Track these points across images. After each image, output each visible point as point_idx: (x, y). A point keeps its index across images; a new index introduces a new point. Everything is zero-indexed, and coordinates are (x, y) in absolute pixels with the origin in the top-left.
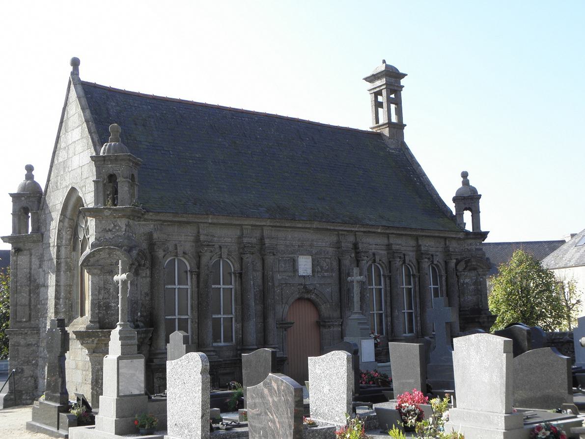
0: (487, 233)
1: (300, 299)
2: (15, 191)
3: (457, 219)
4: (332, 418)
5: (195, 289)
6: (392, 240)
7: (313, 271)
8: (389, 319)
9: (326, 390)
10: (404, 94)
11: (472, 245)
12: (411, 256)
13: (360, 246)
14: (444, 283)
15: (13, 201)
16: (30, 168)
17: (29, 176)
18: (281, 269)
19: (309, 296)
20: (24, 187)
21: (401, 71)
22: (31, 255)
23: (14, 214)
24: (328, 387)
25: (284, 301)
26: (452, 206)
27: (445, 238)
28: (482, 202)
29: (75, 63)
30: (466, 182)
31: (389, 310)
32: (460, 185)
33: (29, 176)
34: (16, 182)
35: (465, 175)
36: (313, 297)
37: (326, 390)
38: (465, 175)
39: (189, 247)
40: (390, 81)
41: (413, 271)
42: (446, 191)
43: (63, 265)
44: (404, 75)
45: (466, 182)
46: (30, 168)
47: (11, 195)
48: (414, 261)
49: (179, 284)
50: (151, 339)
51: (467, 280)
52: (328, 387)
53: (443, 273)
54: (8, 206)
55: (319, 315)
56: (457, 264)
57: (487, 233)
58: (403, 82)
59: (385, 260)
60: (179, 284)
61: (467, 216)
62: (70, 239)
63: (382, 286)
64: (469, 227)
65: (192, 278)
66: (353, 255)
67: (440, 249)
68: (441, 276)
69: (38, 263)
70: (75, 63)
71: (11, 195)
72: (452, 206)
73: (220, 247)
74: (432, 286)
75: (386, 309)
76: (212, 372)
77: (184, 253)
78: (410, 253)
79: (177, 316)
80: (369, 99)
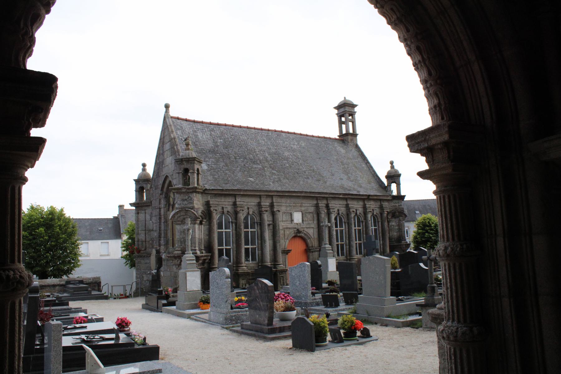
0: (404, 196)
1: (295, 237)
2: (136, 178)
3: (386, 189)
4: (301, 299)
5: (234, 232)
6: (349, 202)
7: (303, 221)
8: (348, 247)
9: (297, 284)
10: (357, 116)
11: (395, 204)
12: (360, 211)
13: (330, 205)
14: (380, 225)
15: (136, 184)
16: (144, 165)
17: (144, 170)
18: (284, 220)
19: (300, 235)
20: (140, 176)
21: (355, 103)
22: (145, 213)
23: (136, 191)
24: (298, 282)
25: (286, 238)
26: (385, 181)
27: (380, 200)
28: (402, 178)
29: (167, 107)
30: (392, 167)
31: (347, 241)
32: (141, 171)
33: (144, 170)
34: (136, 173)
35: (392, 163)
36: (303, 235)
37: (297, 284)
38: (392, 163)
39: (229, 208)
40: (346, 110)
41: (362, 219)
42: (382, 173)
43: (162, 219)
44: (356, 106)
45: (392, 167)
46: (144, 165)
47: (135, 180)
48: (362, 213)
49: (226, 229)
50: (210, 260)
51: (393, 224)
52: (298, 282)
53: (380, 220)
54: (133, 187)
55: (307, 245)
56: (387, 215)
57: (404, 196)
58: (356, 109)
59: (345, 213)
60: (226, 229)
61: (394, 186)
62: (166, 205)
63: (344, 228)
64: (395, 193)
65: (232, 226)
66: (326, 211)
67: (378, 206)
68: (378, 222)
69: (149, 217)
70: (167, 107)
71: (135, 180)
72: (385, 181)
73: (248, 208)
74: (373, 228)
75: (346, 241)
76: (302, 348)
77: (228, 212)
78: (342, 209)
79: (224, 247)
80: (336, 119)
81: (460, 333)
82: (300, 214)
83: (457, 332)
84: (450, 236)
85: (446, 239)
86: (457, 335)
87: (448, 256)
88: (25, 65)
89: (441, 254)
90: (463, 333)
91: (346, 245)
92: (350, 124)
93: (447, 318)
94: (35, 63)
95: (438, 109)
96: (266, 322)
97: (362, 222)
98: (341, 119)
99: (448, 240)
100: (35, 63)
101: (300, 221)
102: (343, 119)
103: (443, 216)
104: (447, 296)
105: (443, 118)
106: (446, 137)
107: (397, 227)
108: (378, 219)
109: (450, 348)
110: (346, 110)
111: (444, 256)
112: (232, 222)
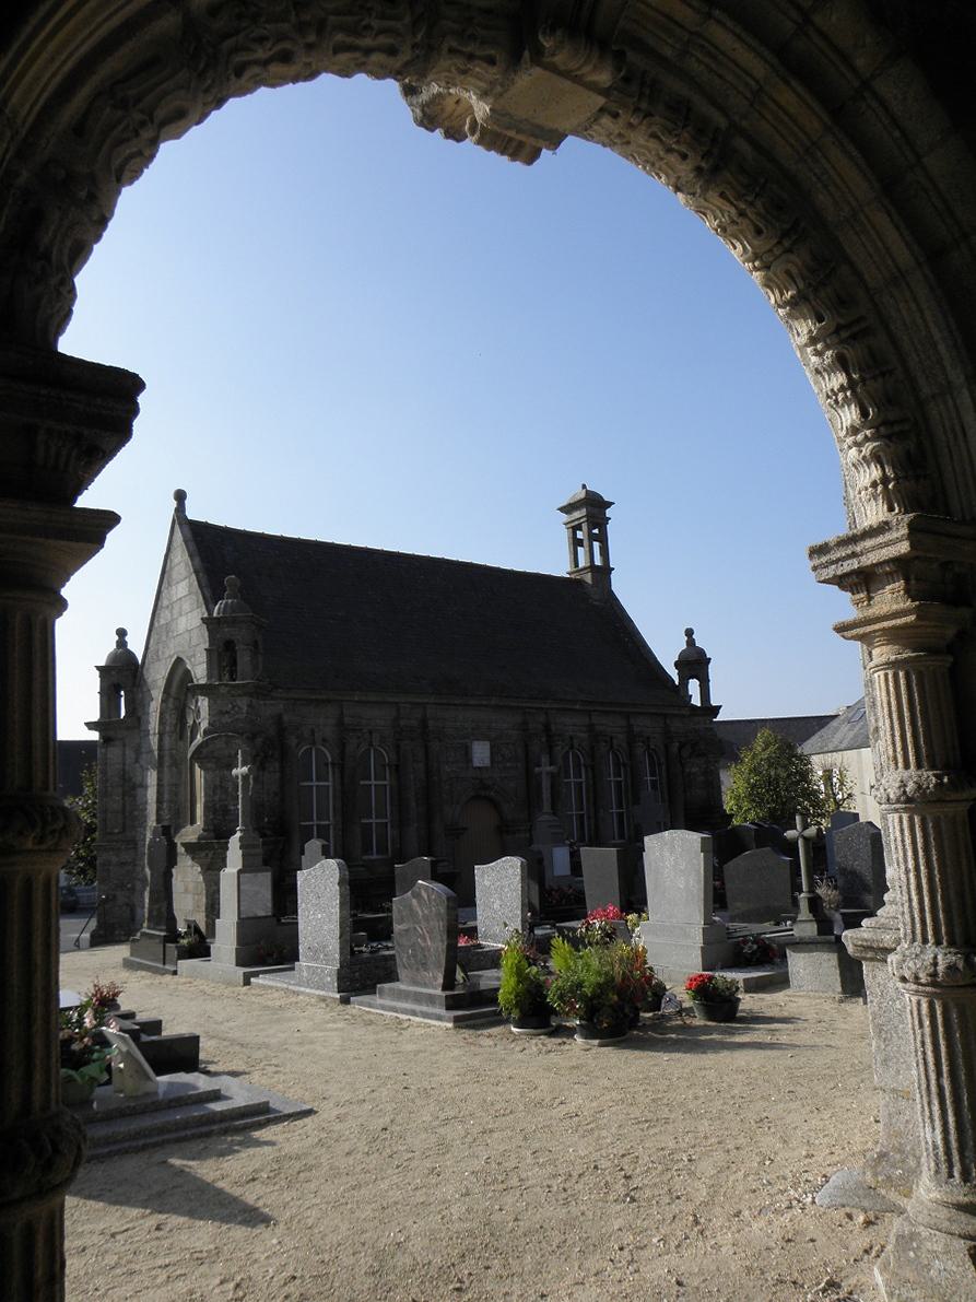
2: (102, 663)
8: (592, 821)
13: (553, 727)
14: (664, 774)
16: (122, 633)
17: (122, 643)
20: (114, 658)
26: (674, 674)
29: (180, 496)
30: (691, 642)
33: (122, 643)
35: (689, 633)
38: (689, 633)
40: (591, 513)
45: (691, 642)
46: (122, 633)
48: (624, 745)
56: (680, 749)
58: (609, 513)
61: (694, 686)
63: (583, 779)
64: (696, 701)
65: (334, 773)
69: (133, 756)
70: (180, 496)
71: (98, 668)
72: (674, 674)
80: (564, 535)
81: (941, 968)
82: (486, 745)
83: (935, 964)
84: (912, 759)
85: (900, 765)
86: (936, 970)
87: (909, 800)
88: (56, 348)
89: (891, 796)
90: (951, 968)
91: (589, 818)
92: (596, 545)
93: (909, 937)
94: (80, 341)
95: (880, 488)
96: (441, 980)
97: (625, 765)
98: (574, 534)
99: (907, 766)
100: (80, 341)
101: (487, 762)
102: (580, 535)
103: (895, 716)
104: (909, 889)
105: (891, 509)
106: (904, 547)
107: (702, 778)
108: (659, 760)
109: (919, 1003)
110: (591, 513)
111: (898, 801)
112: (333, 764)
